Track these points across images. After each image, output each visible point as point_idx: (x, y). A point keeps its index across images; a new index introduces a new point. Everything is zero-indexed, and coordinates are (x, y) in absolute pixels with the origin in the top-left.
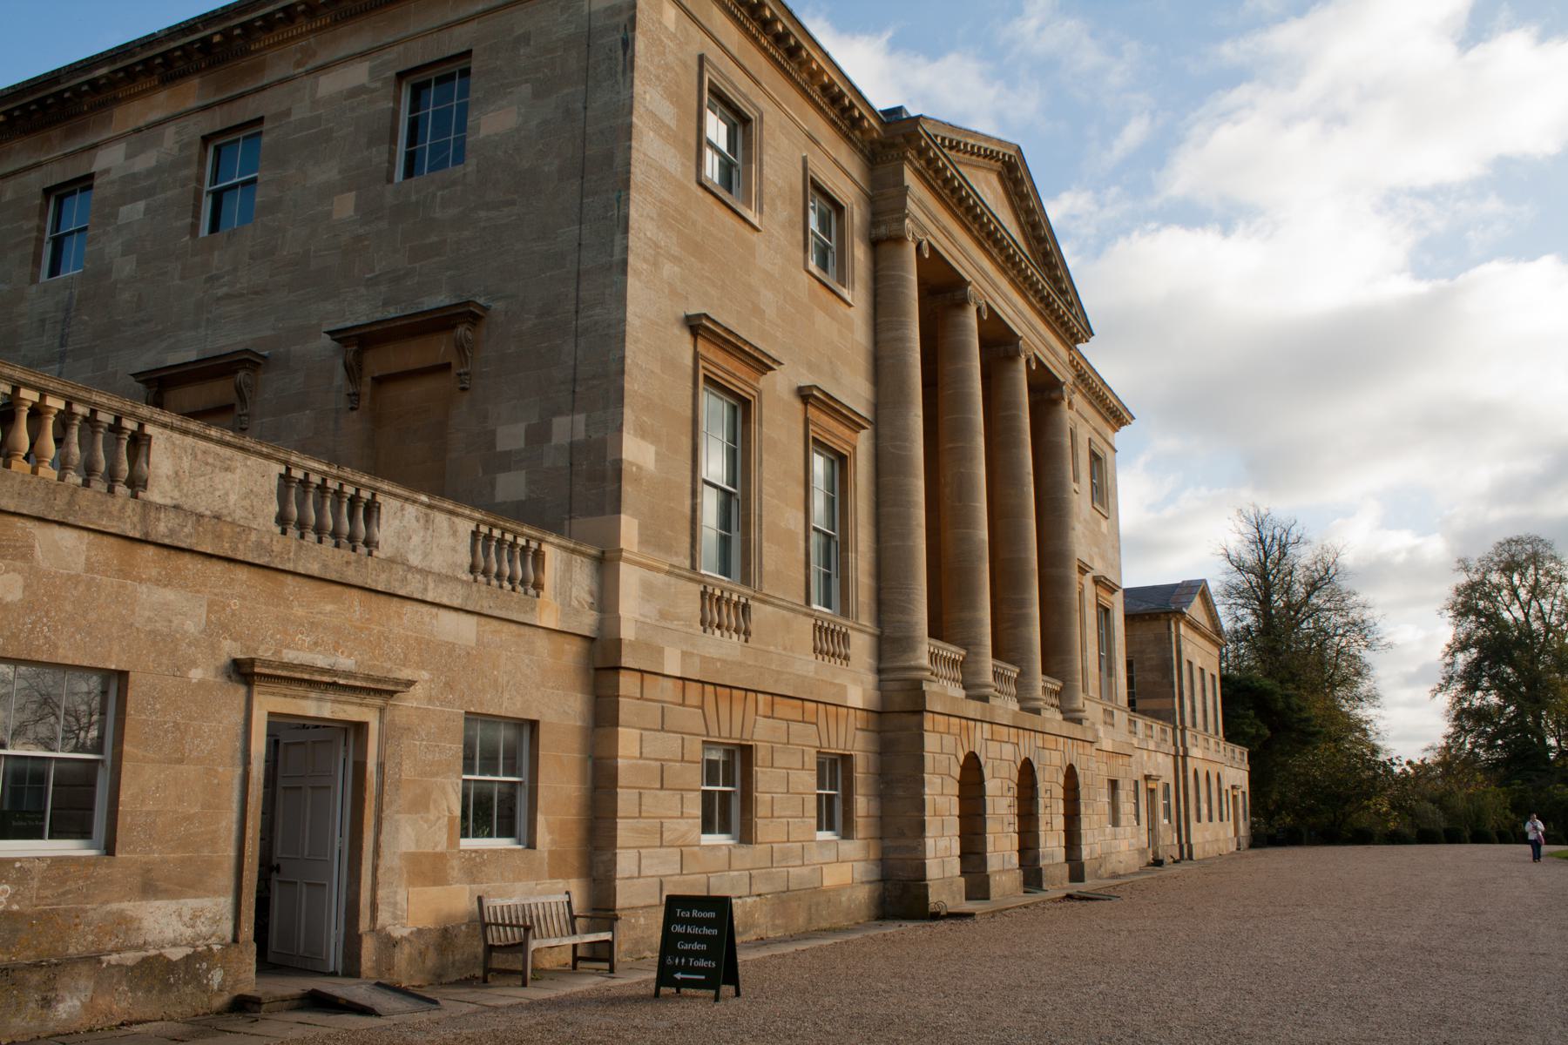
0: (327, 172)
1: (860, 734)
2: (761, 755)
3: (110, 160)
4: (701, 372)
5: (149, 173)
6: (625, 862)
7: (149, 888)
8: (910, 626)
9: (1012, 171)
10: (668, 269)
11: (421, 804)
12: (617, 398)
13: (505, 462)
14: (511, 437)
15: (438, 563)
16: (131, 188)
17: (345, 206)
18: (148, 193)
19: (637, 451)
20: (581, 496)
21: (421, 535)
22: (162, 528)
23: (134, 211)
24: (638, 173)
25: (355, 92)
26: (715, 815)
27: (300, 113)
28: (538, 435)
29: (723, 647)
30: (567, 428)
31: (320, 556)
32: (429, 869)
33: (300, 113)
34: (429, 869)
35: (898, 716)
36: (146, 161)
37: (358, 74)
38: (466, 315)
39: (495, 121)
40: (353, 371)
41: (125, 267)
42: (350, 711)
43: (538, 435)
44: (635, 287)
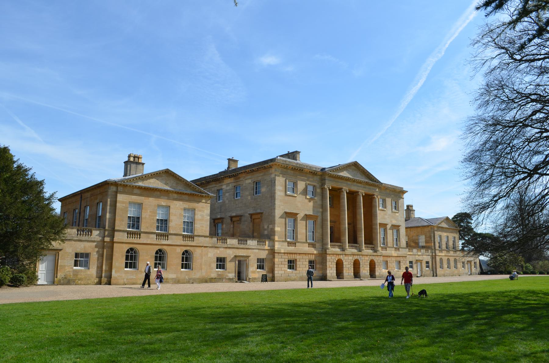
0: (247, 193)
1: (39, 277)
2: (298, 260)
3: (224, 187)
4: (298, 257)
5: (229, 189)
6: (276, 272)
7: (229, 273)
8: (328, 242)
9: (355, 166)
10: (282, 207)
11: (253, 266)
12: (275, 224)
13: (265, 230)
14: (266, 227)
15: (254, 244)
16: (227, 191)
17: (249, 198)
18: (229, 192)
19: (277, 229)
20: (270, 236)
21: (252, 243)
22: (229, 246)
23: (227, 194)
24: (276, 197)
25: (250, 183)
26: (290, 267)
27: (244, 185)
28: (268, 227)
29: (291, 249)
30: (271, 226)
31: (242, 246)
32: (253, 272)
33: (244, 185)
34: (253, 272)
35: (323, 254)
36: (228, 188)
37: (249, 181)
38: (262, 213)
39: (263, 190)
40: (251, 218)
41: (227, 202)
42: (245, 259)
43: (268, 227)
44: (276, 211)
